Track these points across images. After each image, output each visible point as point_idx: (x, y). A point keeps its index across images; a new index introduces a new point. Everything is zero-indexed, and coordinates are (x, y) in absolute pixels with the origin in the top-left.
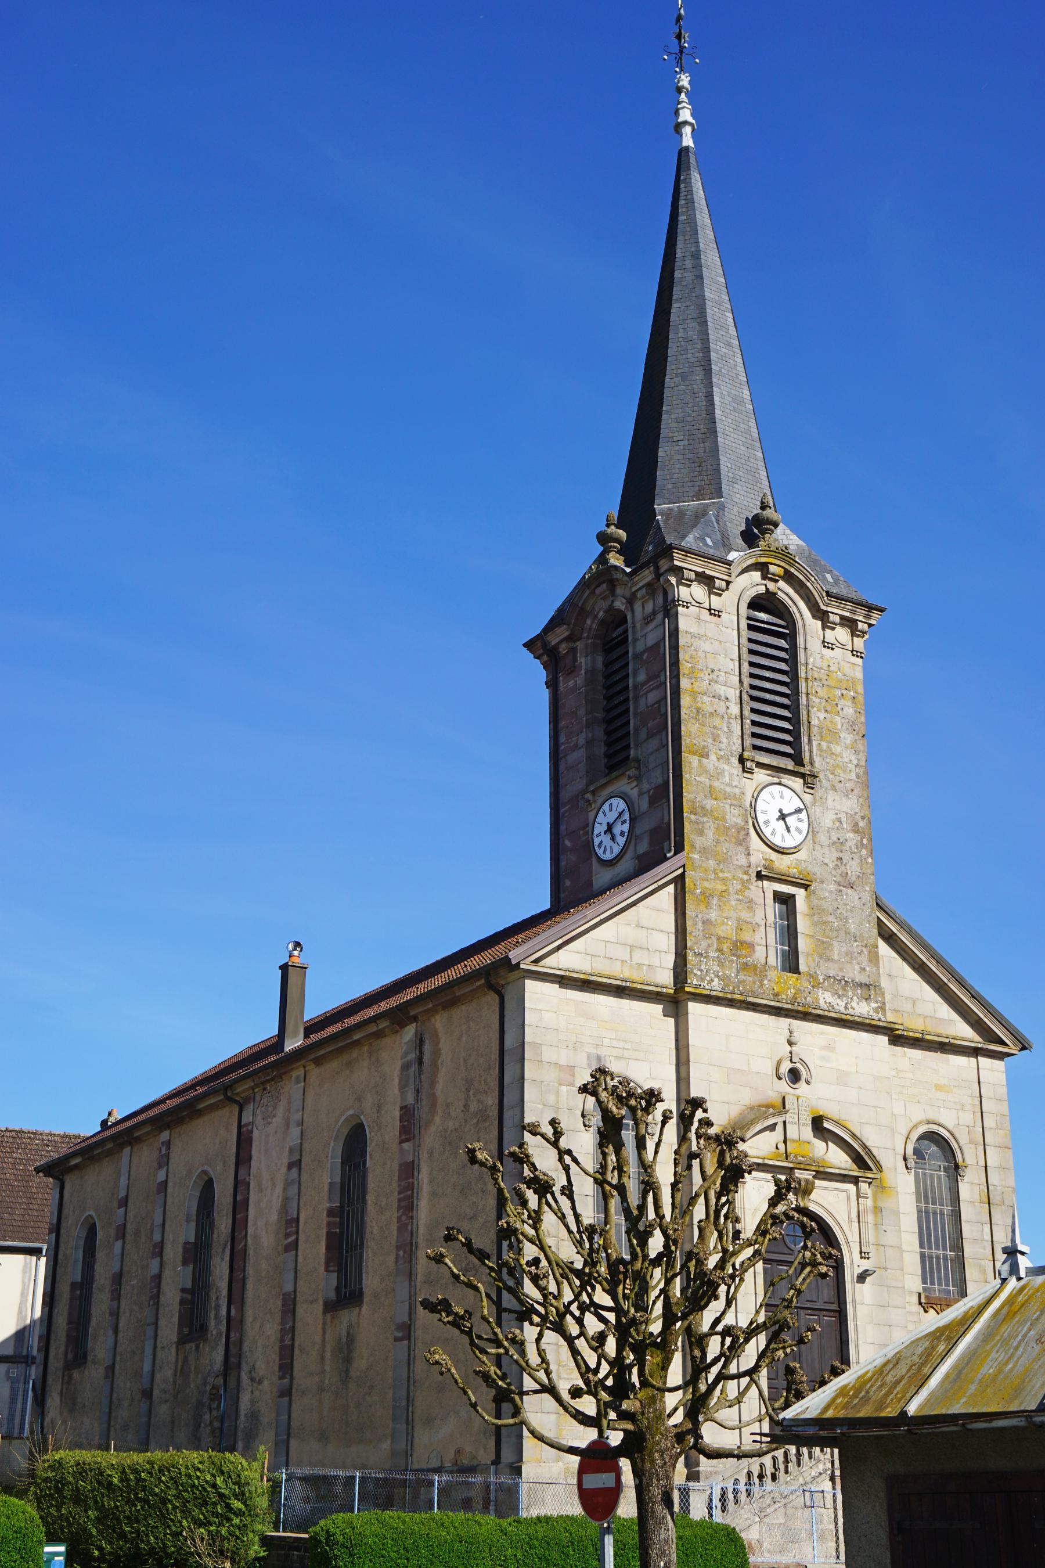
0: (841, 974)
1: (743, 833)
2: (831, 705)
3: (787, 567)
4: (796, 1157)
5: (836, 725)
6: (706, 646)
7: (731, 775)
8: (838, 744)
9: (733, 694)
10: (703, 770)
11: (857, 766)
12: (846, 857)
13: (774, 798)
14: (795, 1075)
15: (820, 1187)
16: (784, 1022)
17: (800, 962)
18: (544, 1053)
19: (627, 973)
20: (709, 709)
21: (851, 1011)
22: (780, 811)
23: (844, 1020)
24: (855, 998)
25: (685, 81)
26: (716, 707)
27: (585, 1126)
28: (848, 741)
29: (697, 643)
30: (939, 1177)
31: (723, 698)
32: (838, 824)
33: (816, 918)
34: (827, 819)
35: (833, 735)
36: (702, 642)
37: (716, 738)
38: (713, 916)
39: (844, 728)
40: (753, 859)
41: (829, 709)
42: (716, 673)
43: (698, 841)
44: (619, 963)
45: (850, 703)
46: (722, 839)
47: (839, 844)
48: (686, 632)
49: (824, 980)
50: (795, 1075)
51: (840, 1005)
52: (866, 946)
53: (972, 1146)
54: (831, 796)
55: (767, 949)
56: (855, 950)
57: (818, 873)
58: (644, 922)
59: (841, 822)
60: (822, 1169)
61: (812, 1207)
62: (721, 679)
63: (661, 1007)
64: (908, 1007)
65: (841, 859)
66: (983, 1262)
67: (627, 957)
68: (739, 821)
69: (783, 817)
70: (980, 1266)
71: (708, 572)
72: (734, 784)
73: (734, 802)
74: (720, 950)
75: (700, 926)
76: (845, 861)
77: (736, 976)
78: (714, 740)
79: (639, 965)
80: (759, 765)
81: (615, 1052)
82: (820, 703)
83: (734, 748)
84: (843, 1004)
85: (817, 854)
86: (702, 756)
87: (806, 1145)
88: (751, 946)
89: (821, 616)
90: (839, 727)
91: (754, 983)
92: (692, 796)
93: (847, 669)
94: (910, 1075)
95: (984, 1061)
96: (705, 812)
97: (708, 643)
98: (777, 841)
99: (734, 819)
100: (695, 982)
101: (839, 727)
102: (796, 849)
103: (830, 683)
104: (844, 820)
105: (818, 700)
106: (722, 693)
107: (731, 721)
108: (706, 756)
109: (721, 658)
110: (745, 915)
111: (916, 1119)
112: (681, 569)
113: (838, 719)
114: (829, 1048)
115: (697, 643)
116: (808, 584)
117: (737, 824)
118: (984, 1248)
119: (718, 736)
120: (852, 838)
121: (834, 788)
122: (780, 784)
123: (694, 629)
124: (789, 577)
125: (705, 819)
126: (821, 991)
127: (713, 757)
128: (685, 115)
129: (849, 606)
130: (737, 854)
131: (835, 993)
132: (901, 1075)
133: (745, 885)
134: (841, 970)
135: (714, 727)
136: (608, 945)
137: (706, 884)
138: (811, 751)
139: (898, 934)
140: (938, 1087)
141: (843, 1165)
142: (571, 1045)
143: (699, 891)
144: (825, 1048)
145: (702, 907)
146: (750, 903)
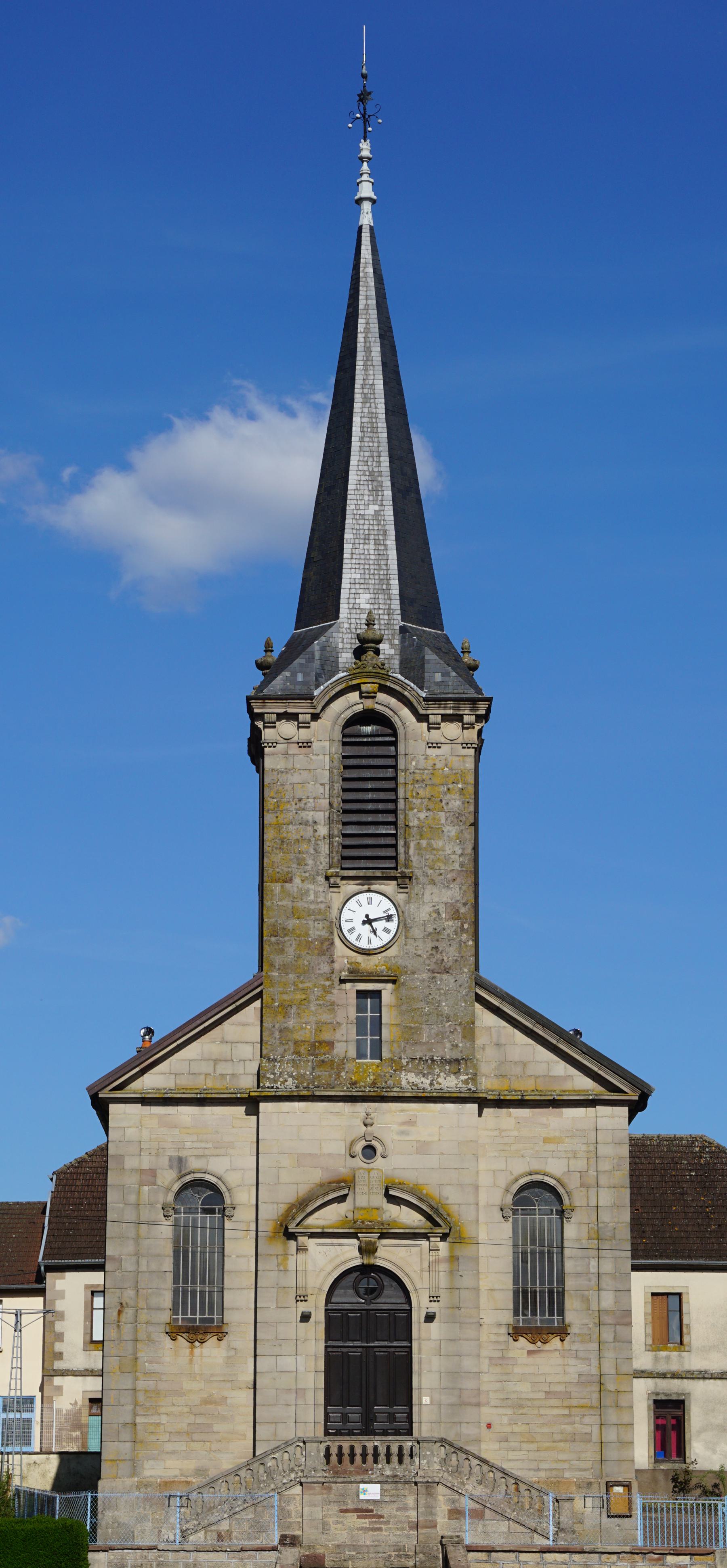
0: (429, 1054)
1: (327, 943)
2: (434, 802)
3: (382, 682)
4: (363, 1222)
5: (439, 820)
6: (295, 778)
7: (316, 893)
8: (440, 838)
9: (321, 817)
10: (286, 894)
11: (461, 855)
12: (442, 946)
13: (360, 905)
14: (370, 1151)
15: (384, 1246)
16: (361, 1108)
17: (383, 1050)
18: (126, 1163)
19: (210, 1084)
20: (294, 836)
22: (367, 916)
23: (421, 1097)
24: (442, 1074)
25: (365, 149)
26: (302, 833)
27: (165, 1216)
28: (453, 833)
29: (282, 778)
31: (311, 822)
33: (404, 1008)
34: (422, 913)
35: (436, 831)
36: (289, 776)
37: (300, 862)
38: (291, 1023)
39: (449, 821)
40: (336, 966)
41: (431, 806)
42: (304, 801)
43: (278, 960)
44: (202, 1077)
45: (457, 796)
46: (304, 953)
48: (273, 770)
49: (408, 1063)
50: (370, 1151)
52: (460, 1024)
53: (584, 1190)
54: (429, 889)
56: (447, 1030)
57: (409, 966)
58: (229, 1038)
59: (439, 913)
60: (385, 1231)
61: (380, 1263)
63: (244, 1108)
65: (437, 947)
66: (586, 1293)
67: (210, 1070)
68: (324, 934)
69: (368, 921)
70: (583, 1296)
71: (290, 711)
72: (319, 900)
73: (319, 917)
74: (297, 1053)
75: (277, 1034)
76: (440, 949)
77: (311, 1074)
78: (299, 864)
79: (223, 1076)
80: (343, 878)
81: (196, 1152)
82: (422, 803)
83: (321, 867)
84: (428, 1081)
85: (410, 948)
86: (286, 882)
87: (375, 1211)
89: (422, 718)
90: (443, 821)
91: (330, 1076)
92: (273, 920)
93: (455, 762)
94: (516, 1133)
96: (286, 932)
97: (296, 775)
98: (363, 944)
99: (318, 933)
100: (267, 1084)
101: (443, 821)
102: (386, 948)
103: (436, 780)
105: (419, 801)
106: (310, 818)
107: (319, 842)
108: (290, 880)
109: (310, 786)
110: (325, 1017)
111: (516, 1173)
112: (262, 714)
113: (442, 815)
114: (411, 1123)
115: (282, 778)
116: (406, 693)
117: (320, 936)
118: (590, 1280)
119: (304, 859)
120: (451, 925)
121: (433, 882)
122: (369, 891)
123: (281, 765)
124: (383, 689)
125: (286, 938)
126: (403, 1073)
127: (297, 881)
128: (366, 190)
129: (451, 704)
130: (319, 964)
132: (503, 1134)
133: (327, 991)
134: (430, 1050)
135: (300, 852)
136: (192, 1063)
137: (285, 997)
138: (407, 853)
139: (501, 1007)
140: (546, 1140)
141: (416, 1224)
142: (153, 1152)
143: (276, 1004)
144: (404, 1123)
145: (280, 1018)
146: (332, 1007)
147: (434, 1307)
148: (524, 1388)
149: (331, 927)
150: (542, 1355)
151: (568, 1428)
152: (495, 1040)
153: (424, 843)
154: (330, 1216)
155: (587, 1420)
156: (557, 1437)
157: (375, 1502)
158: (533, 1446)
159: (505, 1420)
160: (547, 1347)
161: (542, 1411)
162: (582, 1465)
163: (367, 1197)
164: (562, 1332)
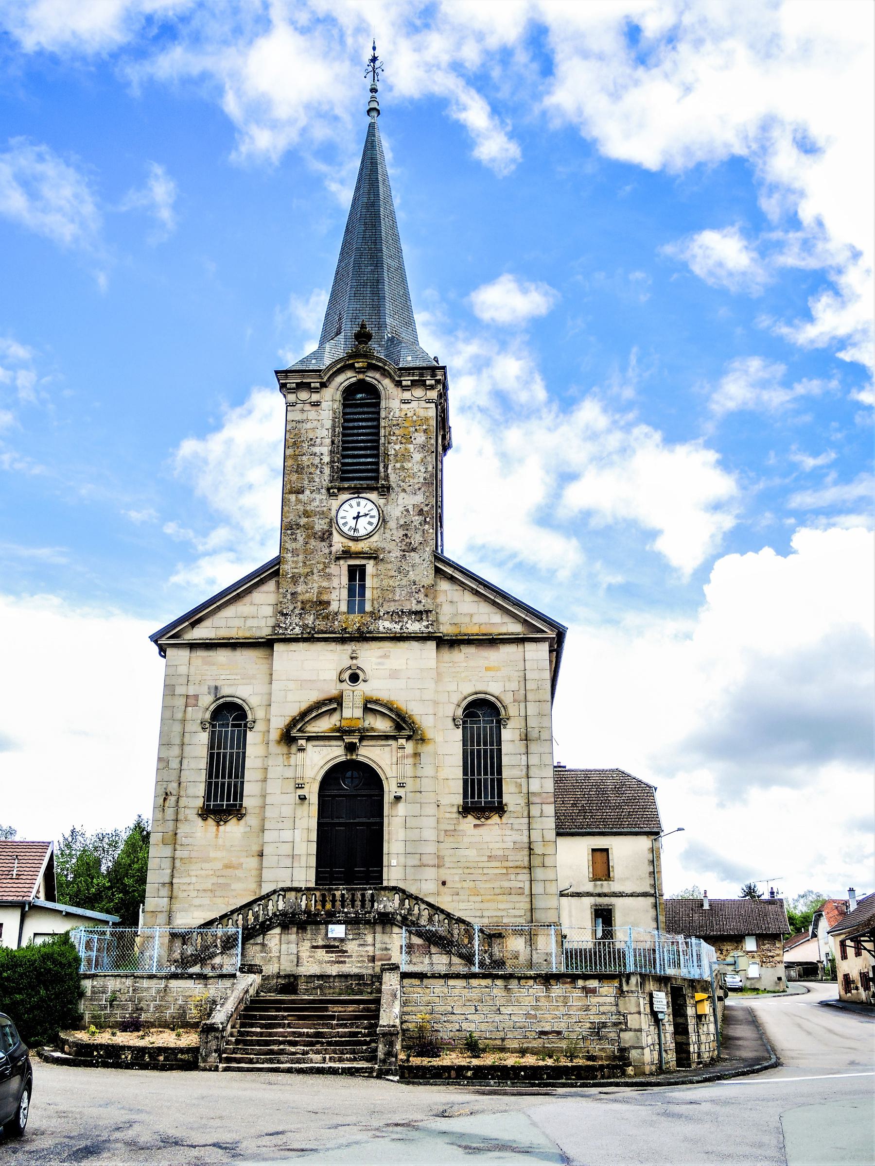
6: (309, 426)
9: (325, 450)
14: (354, 678)
20: (307, 463)
21: (405, 630)
30: (491, 728)
32: (405, 513)
47: (405, 526)
50: (354, 678)
51: (397, 628)
55: (339, 600)
62: (317, 443)
64: (467, 620)
65: (406, 535)
66: (519, 780)
67: (242, 624)
88: (328, 603)
95: (529, 646)
104: (411, 510)
111: (465, 693)
113: (411, 446)
114: (385, 656)
119: (313, 478)
121: (404, 490)
127: (307, 492)
131: (392, 621)
135: (311, 473)
140: (487, 669)
146: (329, 577)
147: (401, 792)
148: (472, 854)
149: (331, 522)
150: (485, 827)
151: (506, 884)
152: (449, 599)
153: (398, 465)
154: (323, 725)
155: (520, 877)
156: (498, 891)
157: (342, 940)
158: (479, 898)
159: (457, 878)
160: (489, 822)
161: (486, 871)
162: (518, 913)
163: (352, 711)
164: (500, 809)
